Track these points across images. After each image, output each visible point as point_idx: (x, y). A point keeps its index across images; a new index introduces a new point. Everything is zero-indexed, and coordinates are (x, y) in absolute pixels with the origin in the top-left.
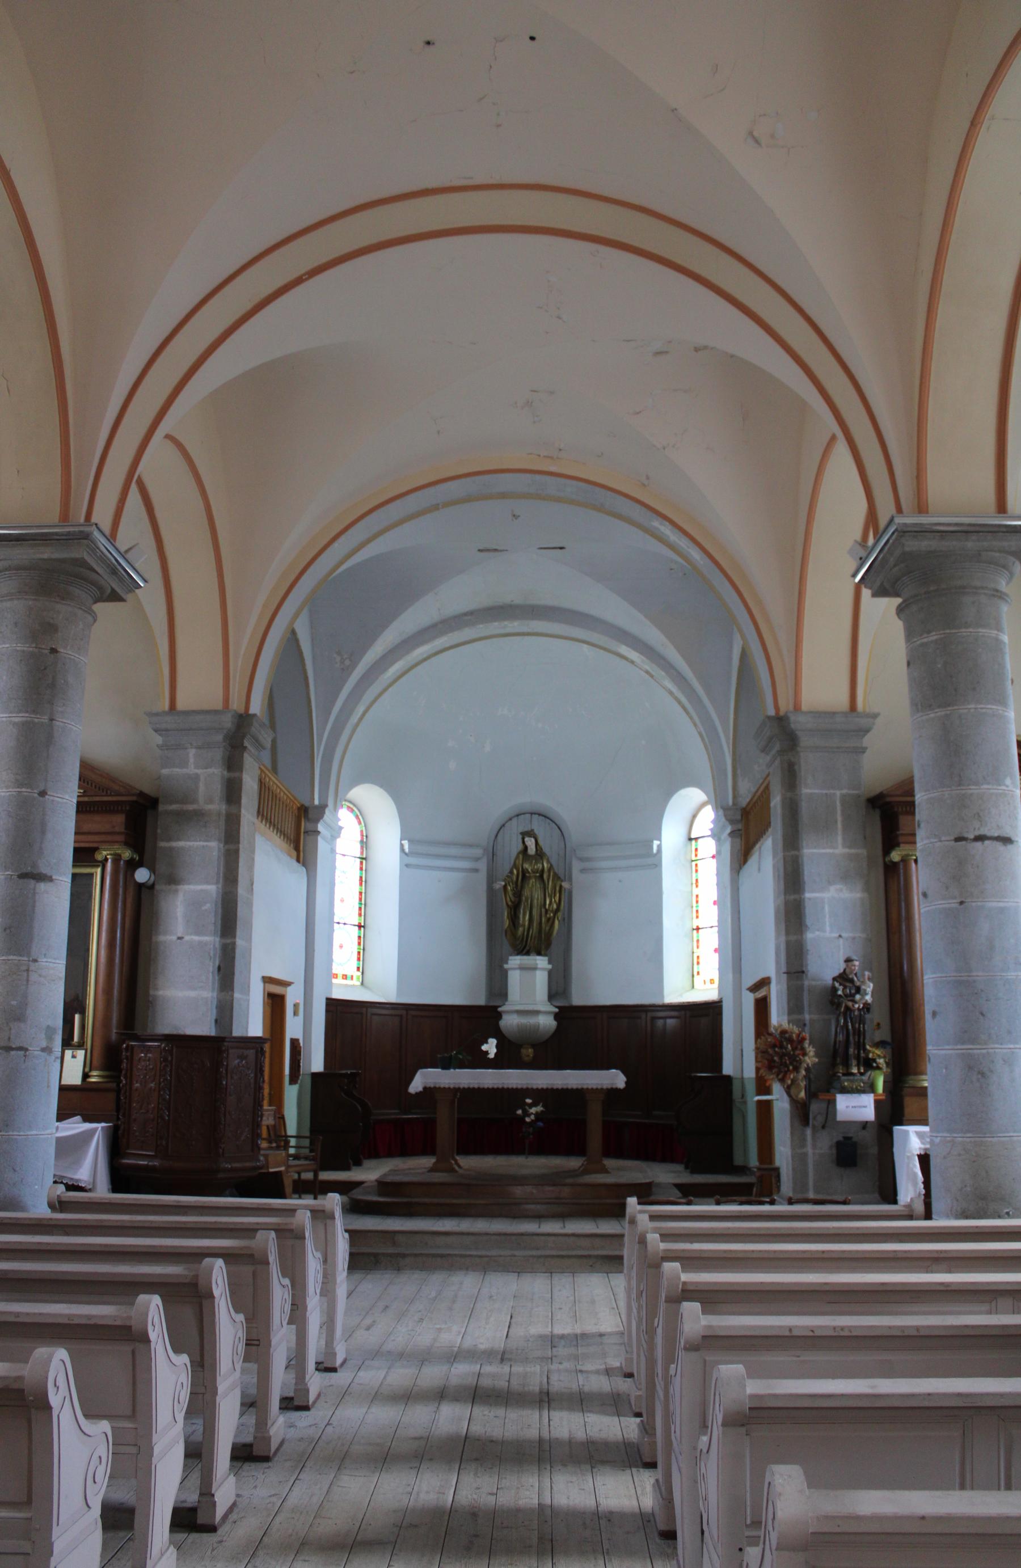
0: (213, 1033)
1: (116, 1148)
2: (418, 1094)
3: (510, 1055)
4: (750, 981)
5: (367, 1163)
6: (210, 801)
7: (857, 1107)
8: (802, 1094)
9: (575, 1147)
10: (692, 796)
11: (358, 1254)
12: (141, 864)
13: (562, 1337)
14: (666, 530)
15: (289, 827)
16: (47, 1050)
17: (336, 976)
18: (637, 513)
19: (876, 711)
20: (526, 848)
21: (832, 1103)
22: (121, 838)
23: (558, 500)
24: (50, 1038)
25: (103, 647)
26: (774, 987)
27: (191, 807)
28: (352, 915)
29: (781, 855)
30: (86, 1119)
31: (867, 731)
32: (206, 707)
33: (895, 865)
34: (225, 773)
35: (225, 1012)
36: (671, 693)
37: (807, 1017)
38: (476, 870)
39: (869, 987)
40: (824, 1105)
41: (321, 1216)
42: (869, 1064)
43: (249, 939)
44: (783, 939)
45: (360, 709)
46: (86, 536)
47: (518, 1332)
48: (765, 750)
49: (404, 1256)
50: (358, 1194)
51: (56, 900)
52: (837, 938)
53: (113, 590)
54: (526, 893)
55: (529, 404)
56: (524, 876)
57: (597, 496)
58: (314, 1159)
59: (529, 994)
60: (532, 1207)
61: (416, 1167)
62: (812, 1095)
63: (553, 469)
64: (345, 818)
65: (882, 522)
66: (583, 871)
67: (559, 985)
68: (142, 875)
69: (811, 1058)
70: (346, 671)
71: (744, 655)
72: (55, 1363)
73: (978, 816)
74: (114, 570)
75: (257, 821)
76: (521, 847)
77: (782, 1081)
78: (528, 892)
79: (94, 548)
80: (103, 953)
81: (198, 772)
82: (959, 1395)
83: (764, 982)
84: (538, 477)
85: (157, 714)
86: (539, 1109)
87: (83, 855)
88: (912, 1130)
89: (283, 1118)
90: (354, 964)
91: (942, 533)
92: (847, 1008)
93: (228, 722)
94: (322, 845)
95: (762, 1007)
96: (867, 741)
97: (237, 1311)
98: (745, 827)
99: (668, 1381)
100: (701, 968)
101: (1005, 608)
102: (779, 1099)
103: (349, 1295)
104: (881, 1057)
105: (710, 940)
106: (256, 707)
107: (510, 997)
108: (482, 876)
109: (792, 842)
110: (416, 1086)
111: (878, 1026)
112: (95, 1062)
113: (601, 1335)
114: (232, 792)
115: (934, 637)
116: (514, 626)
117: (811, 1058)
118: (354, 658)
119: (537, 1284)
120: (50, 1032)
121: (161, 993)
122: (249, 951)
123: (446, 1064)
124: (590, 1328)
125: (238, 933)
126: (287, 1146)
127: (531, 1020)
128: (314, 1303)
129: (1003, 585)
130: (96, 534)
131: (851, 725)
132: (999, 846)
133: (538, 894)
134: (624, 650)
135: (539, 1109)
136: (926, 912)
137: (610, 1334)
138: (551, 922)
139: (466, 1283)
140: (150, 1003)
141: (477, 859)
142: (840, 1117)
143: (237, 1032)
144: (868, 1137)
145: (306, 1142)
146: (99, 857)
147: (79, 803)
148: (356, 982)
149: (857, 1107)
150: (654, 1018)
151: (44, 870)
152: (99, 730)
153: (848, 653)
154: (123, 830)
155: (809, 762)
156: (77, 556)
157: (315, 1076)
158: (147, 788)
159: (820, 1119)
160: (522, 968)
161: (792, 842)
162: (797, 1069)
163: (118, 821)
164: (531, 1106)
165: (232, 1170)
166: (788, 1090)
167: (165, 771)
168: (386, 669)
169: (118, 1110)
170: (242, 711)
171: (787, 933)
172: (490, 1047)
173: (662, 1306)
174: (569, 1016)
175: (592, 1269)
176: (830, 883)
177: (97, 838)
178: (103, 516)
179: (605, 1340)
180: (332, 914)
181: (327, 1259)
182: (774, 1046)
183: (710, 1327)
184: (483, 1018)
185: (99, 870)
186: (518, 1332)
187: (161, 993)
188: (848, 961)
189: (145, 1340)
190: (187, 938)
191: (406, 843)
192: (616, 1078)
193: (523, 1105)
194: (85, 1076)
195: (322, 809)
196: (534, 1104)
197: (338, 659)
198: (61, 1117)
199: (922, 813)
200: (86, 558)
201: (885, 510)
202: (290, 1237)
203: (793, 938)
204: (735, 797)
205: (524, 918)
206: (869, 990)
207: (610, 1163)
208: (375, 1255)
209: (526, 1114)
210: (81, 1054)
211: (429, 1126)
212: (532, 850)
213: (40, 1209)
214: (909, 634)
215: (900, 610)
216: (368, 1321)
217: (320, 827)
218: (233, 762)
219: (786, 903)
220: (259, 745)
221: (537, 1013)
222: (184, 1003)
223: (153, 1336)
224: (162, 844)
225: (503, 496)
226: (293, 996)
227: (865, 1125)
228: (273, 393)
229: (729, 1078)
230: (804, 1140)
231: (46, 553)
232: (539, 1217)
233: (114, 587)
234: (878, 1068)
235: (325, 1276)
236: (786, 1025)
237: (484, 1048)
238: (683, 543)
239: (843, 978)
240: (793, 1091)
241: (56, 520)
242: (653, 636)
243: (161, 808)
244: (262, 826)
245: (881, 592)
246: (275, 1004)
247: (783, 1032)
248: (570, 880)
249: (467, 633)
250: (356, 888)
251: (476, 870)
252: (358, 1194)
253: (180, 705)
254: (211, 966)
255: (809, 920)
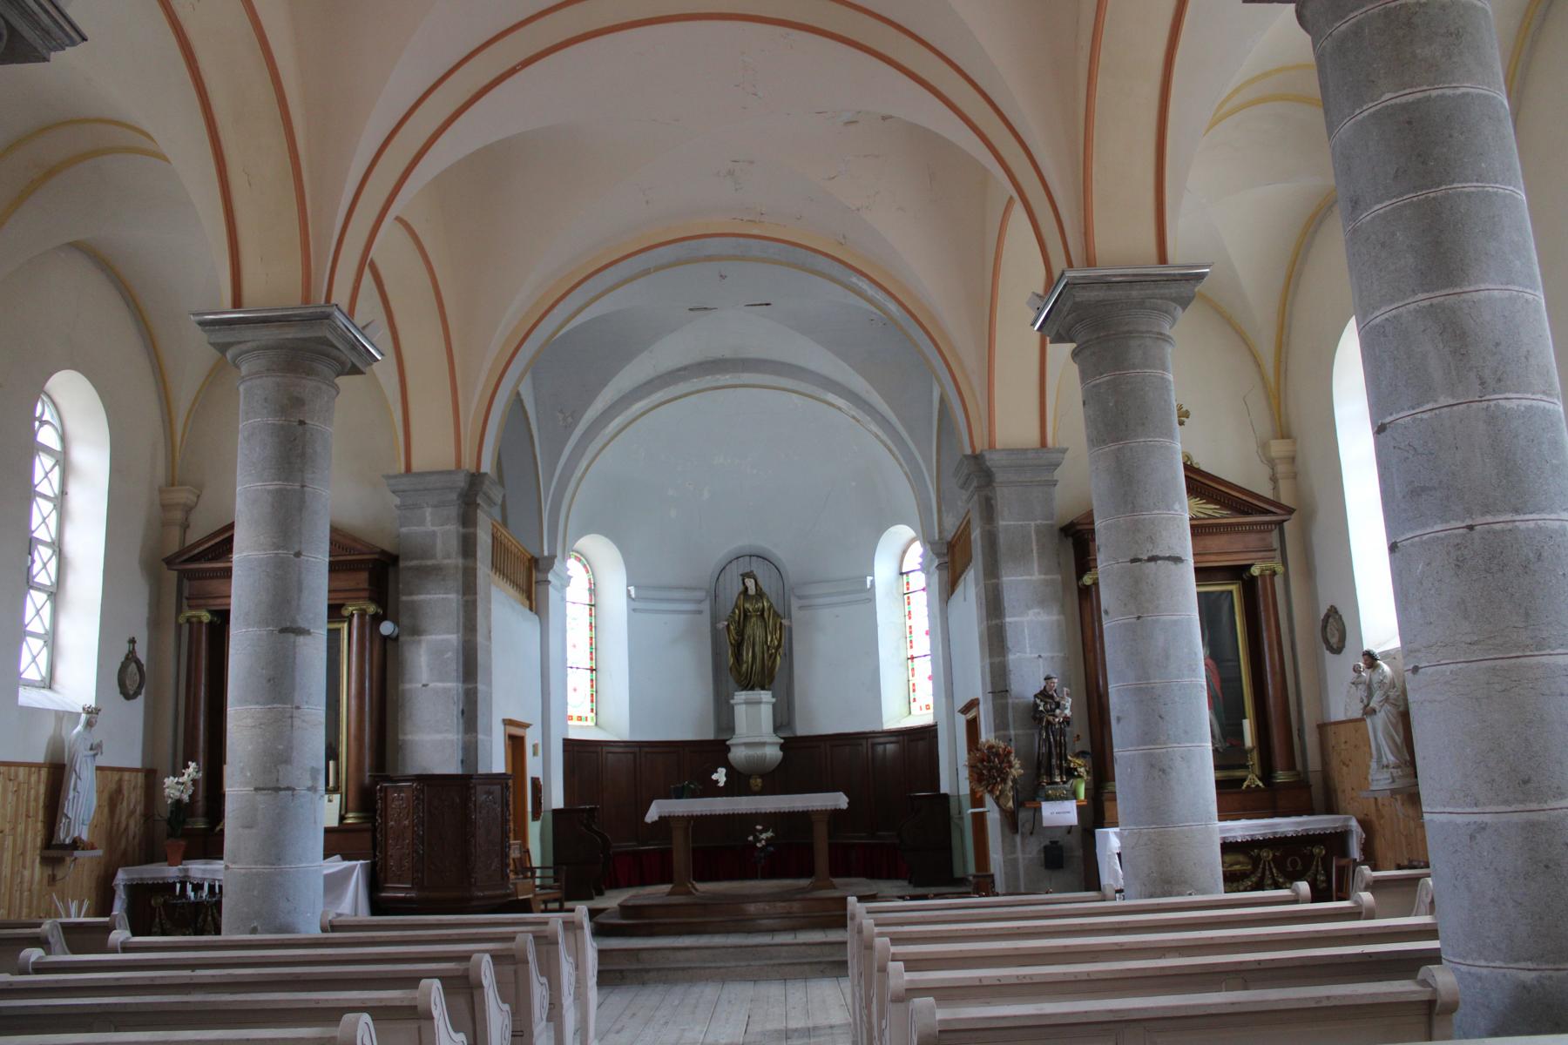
0: (460, 772)
1: (374, 883)
2: (654, 823)
3: (739, 783)
4: (961, 703)
5: (608, 893)
6: (448, 556)
7: (1061, 813)
8: (1011, 804)
9: (806, 871)
10: (902, 533)
11: (609, 971)
12: (384, 618)
13: (796, 1030)
14: (864, 285)
15: (521, 578)
16: (313, 789)
17: (571, 718)
18: (836, 270)
19: (1065, 446)
20: (746, 589)
21: (1038, 810)
22: (366, 594)
23: (764, 260)
24: (314, 778)
25: (346, 415)
26: (981, 707)
27: (429, 563)
28: (587, 660)
29: (982, 584)
30: (345, 858)
31: (1058, 465)
32: (440, 468)
33: (1088, 588)
34: (461, 530)
35: (470, 751)
36: (877, 436)
37: (1012, 732)
38: (700, 612)
39: (1068, 702)
40: (1031, 813)
41: (571, 926)
42: (1070, 773)
43: (489, 684)
44: (987, 661)
45: (583, 464)
46: (328, 316)
47: (755, 1028)
48: (964, 486)
49: (647, 971)
50: (601, 919)
51: (313, 651)
52: (1036, 659)
53: (354, 365)
54: (749, 631)
55: (731, 173)
56: (746, 615)
57: (800, 256)
58: (559, 888)
59: (755, 727)
60: (765, 921)
61: (656, 893)
62: (1019, 804)
63: (755, 232)
64: (574, 567)
65: (1056, 275)
66: (801, 608)
67: (783, 717)
68: (387, 628)
69: (1017, 770)
70: (569, 428)
71: (942, 400)
72: (361, 1025)
73: (1151, 539)
74: (355, 346)
75: (492, 574)
76: (741, 588)
77: (991, 792)
78: (750, 633)
79: (335, 328)
80: (353, 702)
81: (435, 529)
82: (1111, 1011)
83: (973, 704)
84: (741, 240)
85: (395, 477)
86: (770, 834)
87: (335, 611)
88: (1111, 831)
89: (528, 851)
90: (588, 705)
91: (1106, 282)
92: (1049, 722)
93: (461, 481)
94: (553, 593)
95: (973, 727)
96: (1057, 474)
97: (504, 1002)
98: (950, 560)
99: (881, 1032)
100: (918, 695)
101: (1169, 350)
102: (993, 815)
103: (599, 1006)
104: (1081, 766)
105: (924, 668)
106: (487, 466)
107: (737, 731)
108: (706, 619)
109: (992, 571)
110: (652, 815)
111: (1078, 737)
112: (351, 805)
113: (831, 1027)
114: (468, 547)
115: (1105, 378)
116: (727, 379)
117: (1017, 770)
118: (576, 416)
119: (773, 990)
120: (314, 771)
121: (409, 737)
122: (490, 695)
123: (679, 794)
124: (821, 1020)
125: (479, 678)
126: (533, 877)
127: (758, 752)
128: (568, 1000)
129: (1167, 330)
130: (337, 313)
131: (1041, 461)
132: (1170, 565)
133: (759, 632)
134: (831, 397)
135: (770, 834)
136: (1112, 625)
137: (840, 1026)
138: (773, 658)
139: (708, 992)
140: (399, 748)
141: (700, 602)
142: (1045, 824)
143: (482, 770)
144: (1074, 841)
145: (550, 873)
146: (346, 613)
147: (331, 563)
148: (591, 723)
149: (1061, 813)
150: (874, 745)
151: (302, 624)
152: (343, 496)
153: (1031, 394)
154: (366, 586)
155: (1004, 496)
156: (320, 334)
157: (555, 812)
158: (387, 547)
159: (1028, 826)
160: (747, 703)
161: (992, 571)
162: (1004, 781)
163: (362, 578)
164: (761, 832)
165: (484, 898)
166: (997, 800)
167: (404, 530)
168: (606, 426)
169: (374, 848)
170: (473, 470)
171: (991, 656)
172: (720, 776)
173: (876, 974)
174: (795, 747)
175: (823, 974)
176: (1028, 608)
177: (342, 595)
178: (341, 296)
179: (835, 1031)
180: (565, 660)
181: (579, 966)
182: (982, 761)
183: (912, 981)
184: (714, 751)
185: (346, 625)
186: (755, 1028)
187: (409, 737)
188: (1047, 678)
189: (430, 1018)
190: (431, 685)
191: (632, 589)
192: (840, 800)
193: (754, 832)
194: (342, 818)
195: (552, 558)
196: (764, 830)
197: (561, 416)
198: (326, 856)
199: (1100, 539)
200: (329, 336)
201: (1059, 263)
202: (546, 942)
203: (997, 660)
204: (940, 532)
205: (747, 656)
206: (1068, 705)
207: (836, 881)
208: (621, 971)
209: (757, 840)
210: (336, 798)
211: (666, 856)
212: (752, 591)
213: (315, 932)
214: (1084, 376)
215: (1075, 354)
216: (618, 1026)
217: (551, 577)
218: (467, 519)
219: (989, 628)
220: (491, 502)
221: (763, 744)
222: (432, 746)
223: (435, 1013)
224: (404, 598)
225: (710, 258)
226: (532, 737)
227: (1070, 829)
228: (491, 170)
229: (946, 796)
230: (1015, 846)
231: (291, 333)
232: (772, 931)
233: (354, 363)
234: (1079, 776)
235: (577, 981)
236: (993, 741)
237: (714, 777)
238: (880, 296)
239: (1044, 694)
240: (1002, 801)
241: (298, 302)
242: (858, 383)
243: (402, 564)
244: (496, 578)
245: (1059, 339)
246: (516, 745)
247: (991, 747)
248: (790, 617)
249: (683, 387)
250: (586, 634)
251: (700, 612)
252: (601, 919)
253: (415, 467)
254: (455, 710)
255: (1010, 643)
